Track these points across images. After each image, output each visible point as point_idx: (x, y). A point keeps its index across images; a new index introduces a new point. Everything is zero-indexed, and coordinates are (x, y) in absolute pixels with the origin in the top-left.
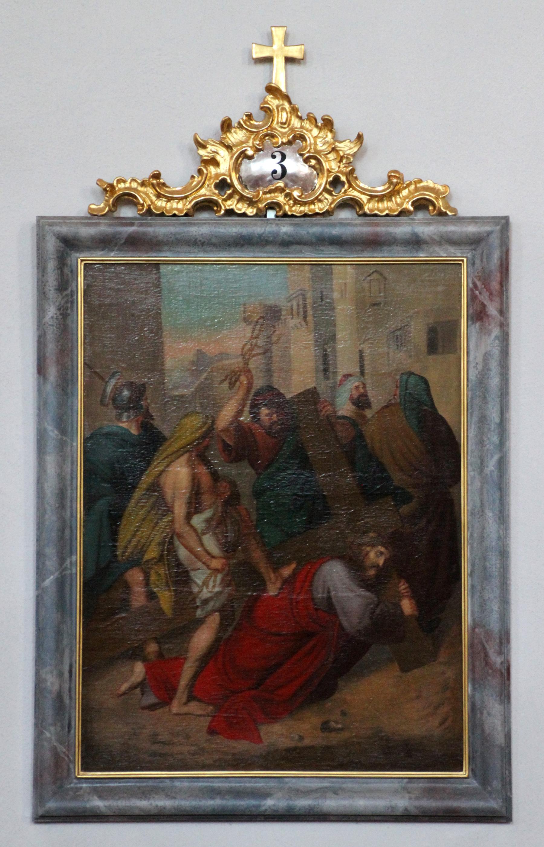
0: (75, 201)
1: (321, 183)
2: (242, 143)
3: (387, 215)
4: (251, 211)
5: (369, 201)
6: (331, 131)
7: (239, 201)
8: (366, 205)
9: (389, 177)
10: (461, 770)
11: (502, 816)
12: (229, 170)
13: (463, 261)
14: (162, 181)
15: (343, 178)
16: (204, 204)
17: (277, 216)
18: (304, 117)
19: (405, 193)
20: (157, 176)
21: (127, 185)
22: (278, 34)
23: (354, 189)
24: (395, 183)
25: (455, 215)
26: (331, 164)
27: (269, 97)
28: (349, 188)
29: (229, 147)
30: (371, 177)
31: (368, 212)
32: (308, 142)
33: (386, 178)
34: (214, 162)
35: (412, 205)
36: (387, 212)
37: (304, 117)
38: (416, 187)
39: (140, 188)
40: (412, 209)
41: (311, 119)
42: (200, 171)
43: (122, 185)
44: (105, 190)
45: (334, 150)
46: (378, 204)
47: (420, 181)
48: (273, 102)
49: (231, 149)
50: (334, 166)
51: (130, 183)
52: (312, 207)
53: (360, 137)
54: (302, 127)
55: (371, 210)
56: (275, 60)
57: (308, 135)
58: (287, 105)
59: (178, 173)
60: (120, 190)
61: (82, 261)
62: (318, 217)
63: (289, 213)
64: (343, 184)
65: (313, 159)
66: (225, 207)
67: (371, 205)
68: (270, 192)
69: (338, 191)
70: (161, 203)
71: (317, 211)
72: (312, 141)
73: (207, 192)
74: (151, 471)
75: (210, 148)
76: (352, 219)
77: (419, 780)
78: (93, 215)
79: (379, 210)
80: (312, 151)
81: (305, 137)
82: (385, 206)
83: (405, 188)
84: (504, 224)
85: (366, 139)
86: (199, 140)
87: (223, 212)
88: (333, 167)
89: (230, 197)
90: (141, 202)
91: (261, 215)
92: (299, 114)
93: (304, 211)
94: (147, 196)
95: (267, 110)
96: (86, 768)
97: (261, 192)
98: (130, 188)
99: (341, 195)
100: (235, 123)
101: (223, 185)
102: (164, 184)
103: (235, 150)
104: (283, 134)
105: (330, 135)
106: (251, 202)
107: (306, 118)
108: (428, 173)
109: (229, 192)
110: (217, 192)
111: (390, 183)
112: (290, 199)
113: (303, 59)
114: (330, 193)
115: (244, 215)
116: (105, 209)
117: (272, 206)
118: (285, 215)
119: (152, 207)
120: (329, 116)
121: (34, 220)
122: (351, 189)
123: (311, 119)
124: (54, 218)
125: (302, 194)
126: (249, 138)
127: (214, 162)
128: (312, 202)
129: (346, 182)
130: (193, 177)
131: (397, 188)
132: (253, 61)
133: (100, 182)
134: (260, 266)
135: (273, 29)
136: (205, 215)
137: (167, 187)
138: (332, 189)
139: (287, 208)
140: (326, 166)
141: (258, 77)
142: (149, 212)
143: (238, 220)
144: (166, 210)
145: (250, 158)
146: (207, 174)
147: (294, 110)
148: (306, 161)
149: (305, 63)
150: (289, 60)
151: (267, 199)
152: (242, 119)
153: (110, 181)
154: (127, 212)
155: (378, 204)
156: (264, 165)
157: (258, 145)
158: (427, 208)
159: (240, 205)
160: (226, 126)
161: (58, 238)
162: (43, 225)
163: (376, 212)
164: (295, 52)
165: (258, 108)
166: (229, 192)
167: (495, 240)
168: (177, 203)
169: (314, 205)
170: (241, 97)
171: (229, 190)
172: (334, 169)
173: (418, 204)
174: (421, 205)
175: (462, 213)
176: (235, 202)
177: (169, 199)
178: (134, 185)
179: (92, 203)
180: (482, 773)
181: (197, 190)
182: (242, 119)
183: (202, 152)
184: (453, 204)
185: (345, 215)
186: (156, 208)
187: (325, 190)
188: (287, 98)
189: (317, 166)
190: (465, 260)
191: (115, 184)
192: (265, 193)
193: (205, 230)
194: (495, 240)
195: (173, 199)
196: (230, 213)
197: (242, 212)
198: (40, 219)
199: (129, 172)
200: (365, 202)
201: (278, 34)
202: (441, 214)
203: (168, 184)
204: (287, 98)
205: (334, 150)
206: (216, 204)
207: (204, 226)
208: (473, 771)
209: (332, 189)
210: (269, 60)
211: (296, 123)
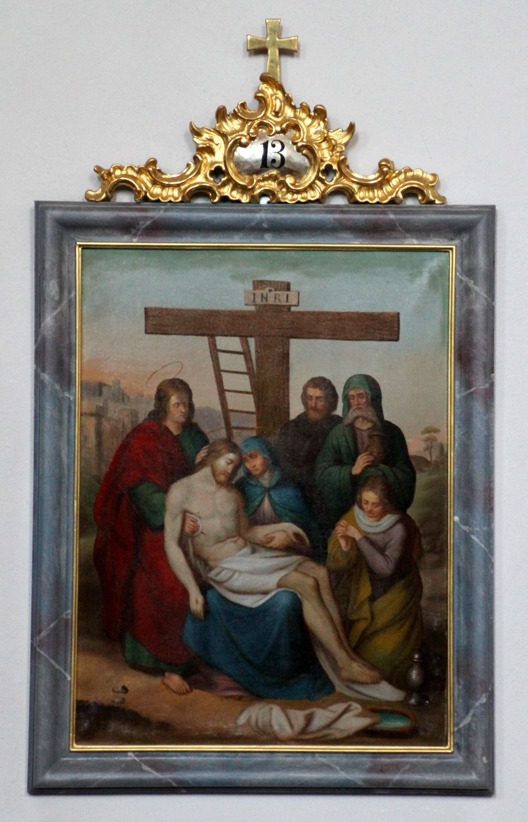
0: (75, 186)
3: (378, 203)
4: (245, 199)
5: (360, 189)
6: (324, 121)
7: (232, 190)
8: (357, 194)
9: (380, 165)
11: (484, 790)
13: (452, 249)
14: (158, 168)
15: (335, 167)
16: (201, 191)
17: (269, 203)
18: (298, 106)
21: (124, 172)
23: (345, 177)
24: (385, 170)
25: (443, 204)
26: (325, 154)
27: (264, 86)
28: (341, 176)
29: (224, 136)
30: (363, 166)
31: (360, 200)
33: (377, 167)
34: (211, 151)
35: (403, 193)
37: (298, 106)
40: (400, 195)
42: (195, 158)
43: (118, 172)
44: (102, 177)
45: (326, 139)
46: (369, 192)
47: (411, 170)
48: (269, 91)
51: (127, 169)
52: (304, 195)
53: (351, 128)
54: (295, 116)
58: (280, 94)
59: (175, 162)
60: (116, 177)
61: (80, 246)
62: (310, 204)
63: (282, 201)
64: (335, 172)
67: (362, 194)
68: (264, 179)
69: (329, 179)
70: (157, 190)
71: (309, 198)
72: (305, 131)
73: (200, 179)
75: (205, 136)
76: (345, 206)
82: (376, 196)
83: (395, 177)
84: (490, 212)
85: (358, 129)
86: (195, 128)
87: (217, 200)
88: (325, 156)
89: (224, 185)
90: (138, 189)
91: (254, 200)
92: (293, 104)
93: (297, 199)
95: (262, 101)
96: (83, 736)
98: (126, 175)
99: (333, 183)
100: (229, 111)
101: (217, 172)
102: (159, 171)
104: (277, 123)
105: (322, 124)
106: (244, 189)
107: (300, 107)
108: (416, 160)
109: (223, 179)
110: (212, 179)
112: (283, 187)
114: (322, 181)
115: (239, 201)
116: (103, 194)
117: (263, 194)
118: (280, 203)
119: (148, 195)
121: (33, 205)
123: (304, 108)
125: (296, 182)
127: (211, 151)
128: (305, 190)
130: (188, 166)
131: (388, 176)
132: (248, 53)
133: (98, 170)
134: (259, 252)
136: (200, 201)
138: (324, 178)
139: (280, 196)
140: (319, 154)
141: (260, 65)
142: (146, 199)
144: (163, 198)
145: (245, 146)
147: (288, 100)
148: (299, 150)
149: (298, 56)
152: (237, 108)
154: (124, 198)
155: (369, 192)
156: (252, 153)
157: (252, 134)
159: (234, 193)
160: (221, 114)
162: (41, 209)
163: (367, 200)
165: (252, 96)
166: (223, 179)
168: (173, 190)
169: (307, 193)
170: (240, 80)
171: (224, 177)
172: (326, 158)
174: (410, 193)
176: (230, 189)
177: (164, 186)
178: (130, 172)
179: (90, 189)
180: (465, 747)
184: (442, 192)
185: (340, 201)
186: (152, 195)
187: (318, 178)
188: (280, 88)
189: (309, 155)
190: (454, 247)
191: (112, 170)
192: (259, 181)
195: (169, 186)
196: (225, 199)
198: (37, 203)
199: (125, 156)
200: (356, 190)
203: (163, 171)
205: (326, 139)
206: (210, 189)
207: (201, 212)
208: (457, 746)
211: (289, 112)
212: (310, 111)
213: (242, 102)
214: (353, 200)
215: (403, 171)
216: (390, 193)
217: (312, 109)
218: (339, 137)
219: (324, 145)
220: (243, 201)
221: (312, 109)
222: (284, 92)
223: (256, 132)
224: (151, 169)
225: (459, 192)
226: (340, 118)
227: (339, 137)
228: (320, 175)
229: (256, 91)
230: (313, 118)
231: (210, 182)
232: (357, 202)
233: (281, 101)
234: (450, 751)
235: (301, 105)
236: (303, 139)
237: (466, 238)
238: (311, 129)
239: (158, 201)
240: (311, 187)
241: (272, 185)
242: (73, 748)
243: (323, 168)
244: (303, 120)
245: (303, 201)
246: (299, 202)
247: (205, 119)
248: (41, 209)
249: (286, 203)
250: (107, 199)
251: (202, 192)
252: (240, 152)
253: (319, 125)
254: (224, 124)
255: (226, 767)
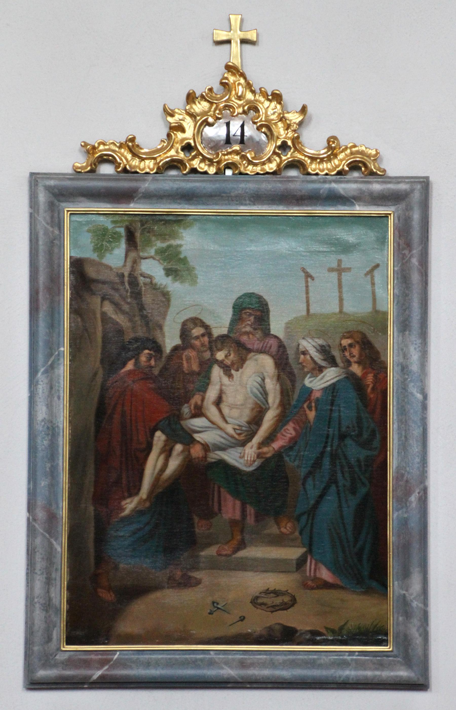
0: (65, 160)
1: (270, 148)
2: (204, 113)
3: (327, 174)
5: (311, 163)
6: (280, 103)
7: (201, 162)
9: (328, 141)
10: (387, 646)
11: (420, 685)
12: (194, 135)
15: (290, 143)
17: (233, 174)
18: (258, 91)
19: (341, 156)
20: (133, 140)
21: (107, 147)
22: (235, 20)
26: (280, 130)
29: (192, 116)
32: (261, 113)
35: (348, 165)
36: (326, 171)
38: (351, 151)
39: (117, 149)
41: (264, 94)
42: (169, 136)
43: (102, 147)
45: (282, 119)
47: (355, 146)
48: (232, 79)
49: (195, 117)
50: (282, 131)
53: (304, 110)
55: (315, 170)
56: (232, 41)
57: (260, 107)
58: (242, 81)
59: (151, 137)
60: (101, 151)
61: (68, 211)
64: (290, 148)
65: (267, 128)
66: (190, 166)
68: (230, 153)
70: (136, 162)
71: (268, 170)
72: (264, 111)
74: (412, 378)
75: (177, 117)
77: (87, 652)
78: (77, 172)
79: (140, 169)
80: (263, 119)
81: (257, 108)
83: (342, 152)
92: (253, 89)
94: (126, 158)
95: (224, 85)
97: (220, 154)
99: (287, 157)
101: (187, 148)
102: (138, 146)
103: (198, 118)
104: (239, 106)
105: (279, 106)
108: (360, 137)
111: (329, 148)
113: (256, 42)
114: (278, 155)
115: (206, 173)
117: (228, 166)
118: (241, 173)
119: (128, 167)
120: (279, 91)
121: (28, 175)
122: (296, 152)
123: (264, 94)
124: (412, 177)
126: (210, 108)
128: (264, 164)
129: (292, 146)
135: (230, 16)
136: (173, 173)
137: (141, 149)
138: (280, 152)
142: (125, 170)
143: (124, 176)
146: (175, 139)
147: (249, 86)
148: (259, 129)
149: (258, 45)
150: (244, 41)
151: (225, 160)
153: (93, 144)
154: (106, 169)
156: (217, 132)
157: (218, 114)
158: (360, 169)
159: (202, 165)
160: (191, 98)
161: (50, 192)
162: (35, 179)
164: (252, 36)
165: (219, 83)
166: (193, 154)
167: (416, 196)
170: (206, 77)
172: (281, 135)
173: (352, 165)
175: (391, 173)
176: (198, 162)
181: (167, 151)
182: (205, 92)
183: (170, 119)
185: (293, 173)
186: (130, 166)
187: (274, 153)
188: (243, 75)
189: (268, 134)
192: (224, 155)
193: (176, 185)
194: (416, 196)
196: (194, 171)
197: (205, 170)
198: (32, 174)
199: (108, 133)
201: (235, 20)
202: (372, 174)
203: (142, 146)
204: (243, 75)
206: (181, 162)
209: (280, 152)
210: (228, 42)
211: (249, 96)
212: (268, 96)
213: (210, 87)
214: (305, 172)
215: (349, 146)
216: (338, 166)
217: (270, 93)
218: (294, 118)
219: (280, 125)
220: (210, 172)
221: (270, 93)
222: (245, 78)
223: (221, 113)
224: (130, 144)
225: (397, 165)
226: (293, 100)
227: (294, 118)
228: (277, 151)
229: (221, 77)
230: (270, 101)
231: (182, 155)
232: (309, 174)
233: (243, 87)
234: (391, 649)
235: (260, 89)
236: (262, 119)
237: (402, 206)
238: (269, 109)
239: (137, 173)
240: (269, 160)
241: (237, 158)
242: (64, 647)
243: (279, 143)
244: (262, 103)
245: (262, 172)
246: (258, 174)
247: (177, 102)
248: (35, 179)
249: (247, 174)
250: (92, 171)
251: (174, 164)
252: (209, 132)
253: (276, 107)
254: (194, 106)
255: (170, 664)
